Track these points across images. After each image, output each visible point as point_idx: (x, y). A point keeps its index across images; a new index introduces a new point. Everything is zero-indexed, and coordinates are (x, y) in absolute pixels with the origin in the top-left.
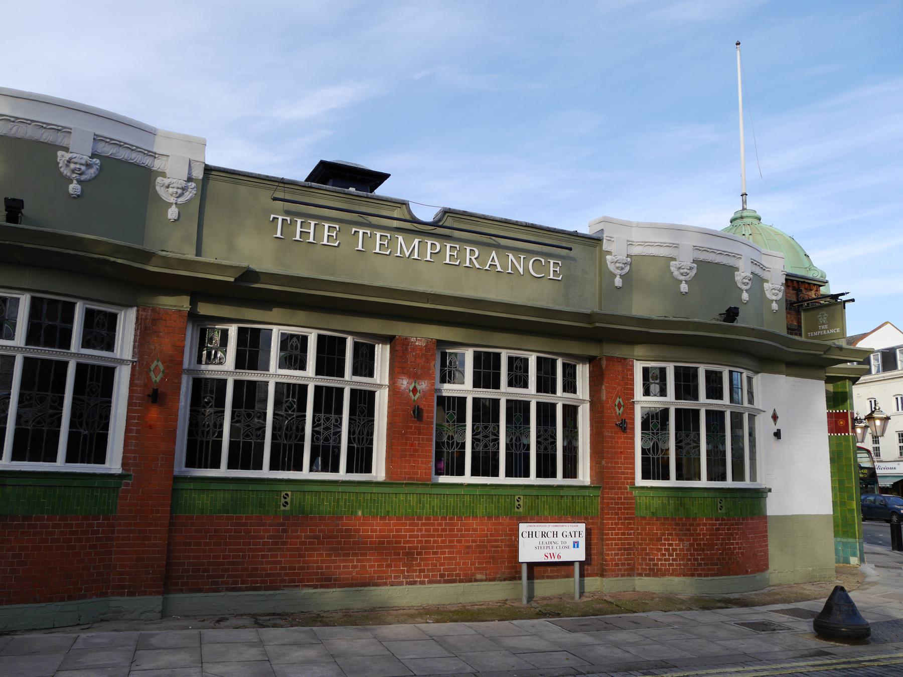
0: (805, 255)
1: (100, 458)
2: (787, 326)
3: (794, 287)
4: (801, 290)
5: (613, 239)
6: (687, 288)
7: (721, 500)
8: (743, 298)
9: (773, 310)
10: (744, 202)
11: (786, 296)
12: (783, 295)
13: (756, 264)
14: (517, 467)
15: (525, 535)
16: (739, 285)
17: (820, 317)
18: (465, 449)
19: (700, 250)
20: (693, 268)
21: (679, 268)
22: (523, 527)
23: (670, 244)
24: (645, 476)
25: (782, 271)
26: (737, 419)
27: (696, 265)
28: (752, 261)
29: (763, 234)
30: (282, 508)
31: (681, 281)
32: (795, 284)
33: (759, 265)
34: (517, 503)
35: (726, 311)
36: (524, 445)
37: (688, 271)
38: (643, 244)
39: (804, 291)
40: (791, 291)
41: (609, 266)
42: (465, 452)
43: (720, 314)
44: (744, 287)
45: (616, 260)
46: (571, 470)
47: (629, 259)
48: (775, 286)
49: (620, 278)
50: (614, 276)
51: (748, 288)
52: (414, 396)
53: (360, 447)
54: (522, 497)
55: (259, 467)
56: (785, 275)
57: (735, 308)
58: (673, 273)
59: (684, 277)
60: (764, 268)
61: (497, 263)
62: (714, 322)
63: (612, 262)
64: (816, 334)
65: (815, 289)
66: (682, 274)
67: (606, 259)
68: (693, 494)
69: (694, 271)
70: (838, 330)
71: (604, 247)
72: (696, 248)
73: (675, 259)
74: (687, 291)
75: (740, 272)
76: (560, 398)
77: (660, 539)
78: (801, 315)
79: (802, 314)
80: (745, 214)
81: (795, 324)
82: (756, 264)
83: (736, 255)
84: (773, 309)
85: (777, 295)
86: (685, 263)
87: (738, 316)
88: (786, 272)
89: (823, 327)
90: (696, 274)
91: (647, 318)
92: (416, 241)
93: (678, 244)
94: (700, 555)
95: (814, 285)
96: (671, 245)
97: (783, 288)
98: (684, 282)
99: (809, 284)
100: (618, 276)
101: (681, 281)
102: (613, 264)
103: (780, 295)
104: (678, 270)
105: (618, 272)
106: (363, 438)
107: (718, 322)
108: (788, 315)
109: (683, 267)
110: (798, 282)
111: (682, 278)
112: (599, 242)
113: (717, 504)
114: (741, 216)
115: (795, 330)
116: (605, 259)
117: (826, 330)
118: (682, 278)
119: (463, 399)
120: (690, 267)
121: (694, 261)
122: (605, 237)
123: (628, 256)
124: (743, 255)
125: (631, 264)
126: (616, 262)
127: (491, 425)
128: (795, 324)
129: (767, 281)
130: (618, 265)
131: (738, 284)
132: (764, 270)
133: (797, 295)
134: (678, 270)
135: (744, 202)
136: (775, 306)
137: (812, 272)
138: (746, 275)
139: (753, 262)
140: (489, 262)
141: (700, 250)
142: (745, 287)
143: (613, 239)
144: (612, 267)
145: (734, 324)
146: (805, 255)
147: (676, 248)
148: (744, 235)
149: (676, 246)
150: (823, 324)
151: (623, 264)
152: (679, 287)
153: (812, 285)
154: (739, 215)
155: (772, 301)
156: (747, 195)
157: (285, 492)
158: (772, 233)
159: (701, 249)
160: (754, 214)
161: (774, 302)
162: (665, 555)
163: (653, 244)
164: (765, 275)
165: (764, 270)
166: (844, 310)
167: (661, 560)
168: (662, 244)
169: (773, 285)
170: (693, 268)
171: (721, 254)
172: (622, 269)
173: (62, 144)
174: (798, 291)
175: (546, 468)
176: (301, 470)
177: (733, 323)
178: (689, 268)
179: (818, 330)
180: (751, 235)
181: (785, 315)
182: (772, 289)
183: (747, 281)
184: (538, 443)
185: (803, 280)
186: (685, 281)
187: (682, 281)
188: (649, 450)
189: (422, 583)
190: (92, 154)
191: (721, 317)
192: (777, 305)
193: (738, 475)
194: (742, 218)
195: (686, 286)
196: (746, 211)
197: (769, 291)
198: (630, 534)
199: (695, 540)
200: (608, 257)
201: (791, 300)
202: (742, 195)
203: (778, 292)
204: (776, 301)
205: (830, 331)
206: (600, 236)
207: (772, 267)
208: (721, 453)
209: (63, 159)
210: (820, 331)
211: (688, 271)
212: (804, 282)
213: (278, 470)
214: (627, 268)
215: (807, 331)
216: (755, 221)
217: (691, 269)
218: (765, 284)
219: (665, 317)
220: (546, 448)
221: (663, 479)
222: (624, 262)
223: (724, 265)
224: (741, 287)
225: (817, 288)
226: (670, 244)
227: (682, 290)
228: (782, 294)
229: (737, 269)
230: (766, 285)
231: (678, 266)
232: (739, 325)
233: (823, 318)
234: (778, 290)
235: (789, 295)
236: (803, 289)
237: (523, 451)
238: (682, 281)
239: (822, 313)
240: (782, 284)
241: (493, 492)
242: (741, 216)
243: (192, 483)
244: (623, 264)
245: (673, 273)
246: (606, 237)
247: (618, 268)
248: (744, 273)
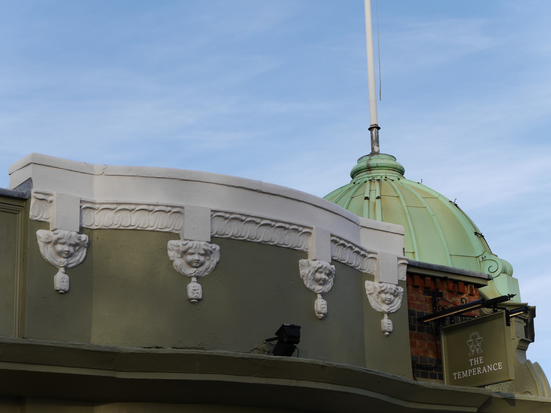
0: (476, 233)
2: (414, 363)
3: (428, 288)
4: (441, 295)
5: (50, 198)
6: (200, 291)
8: (315, 308)
9: (384, 332)
10: (375, 141)
11: (409, 304)
12: (402, 303)
13: (343, 245)
16: (308, 284)
17: (470, 343)
19: (226, 219)
20: (211, 252)
23: (167, 206)
25: (399, 259)
27: (218, 247)
29: (401, 197)
31: (188, 279)
32: (429, 283)
33: (350, 247)
35: (276, 334)
37: (202, 259)
39: (447, 297)
40: (422, 296)
41: (42, 250)
43: (267, 340)
44: (318, 288)
45: (55, 237)
47: (84, 237)
48: (385, 286)
49: (65, 273)
50: (54, 269)
51: (326, 291)
56: (406, 267)
57: (292, 327)
58: (172, 261)
59: (195, 269)
60: (363, 253)
62: (256, 355)
63: (49, 243)
64: (465, 374)
65: (469, 292)
66: (190, 264)
69: (215, 258)
70: (499, 365)
71: (31, 213)
72: (216, 214)
73: (176, 236)
74: (200, 297)
75: (309, 259)
78: (440, 339)
79: (443, 338)
80: (375, 161)
81: (431, 356)
82: (343, 245)
83: (300, 229)
84: (383, 329)
85: (391, 302)
86: (195, 243)
87: (298, 342)
88: (407, 260)
89: (476, 361)
90: (217, 263)
91: (107, 350)
92: (466, 371)
93: (182, 207)
95: (466, 283)
96: (169, 209)
97: (401, 289)
98: (194, 279)
99: (456, 282)
100: (62, 270)
101: (188, 279)
102: (50, 246)
103: (397, 303)
104: (182, 257)
105: (61, 261)
107: (265, 356)
108: (418, 342)
109: (190, 251)
110: (433, 278)
111: (190, 271)
112: (24, 204)
114: (368, 165)
115: (431, 368)
116: (35, 238)
117: (481, 366)
118: (190, 271)
120: (205, 250)
121: (214, 239)
122: (33, 194)
123: (82, 230)
124: (314, 227)
125: (89, 246)
126: (56, 242)
128: (431, 356)
129: (371, 278)
130: (59, 247)
131: (305, 282)
132: (364, 256)
133: (434, 303)
134: (182, 257)
135: (375, 141)
136: (386, 323)
137: (488, 264)
138: (320, 265)
139: (336, 241)
140: (483, 370)
141: (226, 219)
142: (320, 287)
143: (50, 198)
144: (47, 252)
145: (293, 358)
146: (476, 233)
147: (178, 215)
148: (367, 198)
149: (179, 211)
150: (476, 355)
151: (70, 245)
152: (186, 290)
153: (461, 285)
154: (363, 164)
155: (382, 314)
156: (379, 128)
158: (418, 195)
159: (227, 215)
160: (391, 162)
161: (386, 316)
163: (133, 207)
164: (367, 266)
165: (364, 256)
166: (507, 328)
168: (151, 208)
169: (381, 285)
170: (211, 252)
172: (69, 255)
173: (123, 214)
174: (435, 295)
177: (291, 356)
178: (202, 252)
179: (468, 366)
180: (378, 198)
181: (408, 341)
182: (380, 293)
183: (323, 276)
185: (442, 275)
186: (197, 277)
187: (190, 277)
190: (212, 237)
191: (271, 345)
192: (390, 322)
194: (369, 168)
195: (198, 286)
196: (375, 156)
197: (374, 295)
200: (41, 234)
201: (423, 313)
202: (370, 129)
203: (392, 297)
204: (389, 314)
205: (487, 368)
206: (24, 192)
207: (378, 252)
210: (471, 368)
211: (202, 259)
212: (445, 279)
214: (81, 255)
215: (452, 370)
216: (393, 175)
217: (207, 253)
218: (367, 282)
219: (157, 348)
222: (73, 242)
223: (275, 246)
224: (312, 287)
225: (471, 290)
226: (167, 206)
227: (190, 295)
228: (400, 301)
229: (304, 254)
230: (369, 285)
231: (182, 248)
232: (301, 359)
233: (475, 343)
234: (391, 294)
235: (418, 303)
236: (445, 292)
238: (190, 277)
239: (473, 334)
240: (400, 283)
242: (368, 165)
244: (70, 245)
245: (172, 261)
246: (35, 193)
247: (60, 253)
248: (317, 261)
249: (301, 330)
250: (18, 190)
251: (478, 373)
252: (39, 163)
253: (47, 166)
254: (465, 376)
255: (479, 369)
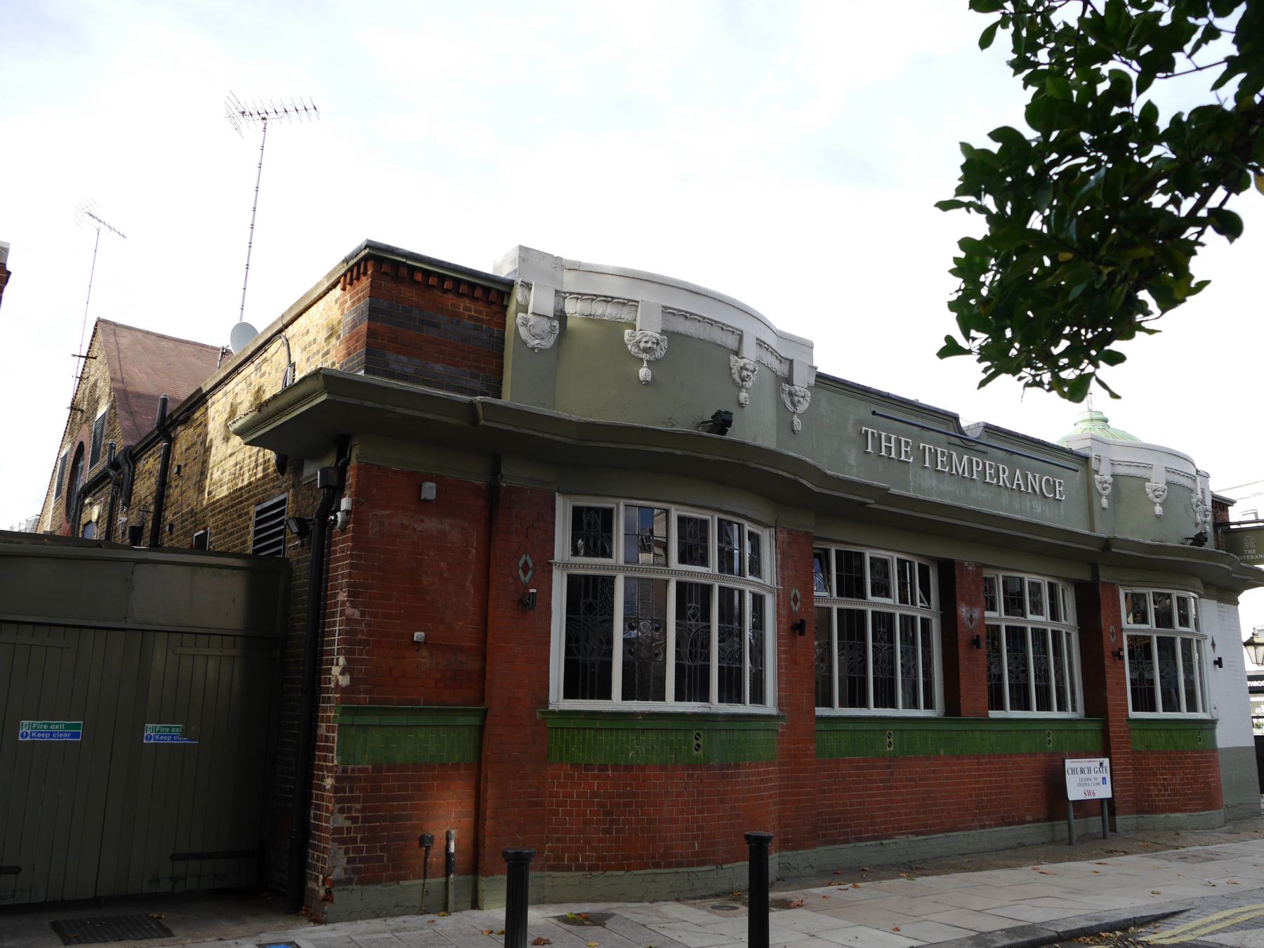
1: (1135, 709)
7: (698, 734)
14: (1171, 705)
15: (1070, 771)
16: (626, 341)
18: (709, 661)
21: (1155, 490)
22: (1069, 764)
24: (570, 693)
26: (1187, 644)
28: (758, 342)
30: (1199, 743)
34: (891, 740)
35: (712, 418)
36: (1147, 680)
38: (1129, 464)
42: (709, 666)
45: (1104, 480)
46: (758, 697)
52: (525, 576)
53: (1143, 687)
54: (701, 733)
55: (607, 695)
57: (727, 413)
61: (1021, 482)
67: (1094, 478)
68: (753, 725)
73: (1149, 480)
76: (748, 586)
77: (1155, 774)
89: (1250, 552)
94: (1188, 789)
106: (696, 652)
113: (894, 741)
116: (1094, 479)
119: (707, 589)
127: (1021, 655)
139: (1168, 470)
145: (1203, 548)
150: (1250, 548)
157: (697, 732)
162: (1160, 790)
167: (1157, 795)
171: (1144, 467)
175: (731, 691)
176: (663, 699)
184: (1161, 677)
185: (1219, 500)
188: (1136, 679)
189: (990, 826)
192: (1161, 509)
193: (1192, 707)
198: (1129, 770)
199: (1185, 773)
208: (1147, 682)
209: (737, 364)
210: (1245, 555)
213: (648, 700)
220: (1017, 678)
221: (1150, 711)
231: (1154, 488)
237: (994, 682)
241: (1170, 727)
243: (598, 721)
249: (733, 416)
250: (1079, 451)
251: (1001, 483)
252: (739, 311)
253: (663, 284)
254: (960, 471)
255: (1248, 556)
